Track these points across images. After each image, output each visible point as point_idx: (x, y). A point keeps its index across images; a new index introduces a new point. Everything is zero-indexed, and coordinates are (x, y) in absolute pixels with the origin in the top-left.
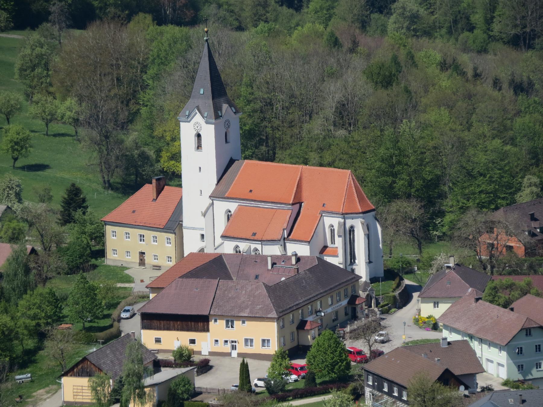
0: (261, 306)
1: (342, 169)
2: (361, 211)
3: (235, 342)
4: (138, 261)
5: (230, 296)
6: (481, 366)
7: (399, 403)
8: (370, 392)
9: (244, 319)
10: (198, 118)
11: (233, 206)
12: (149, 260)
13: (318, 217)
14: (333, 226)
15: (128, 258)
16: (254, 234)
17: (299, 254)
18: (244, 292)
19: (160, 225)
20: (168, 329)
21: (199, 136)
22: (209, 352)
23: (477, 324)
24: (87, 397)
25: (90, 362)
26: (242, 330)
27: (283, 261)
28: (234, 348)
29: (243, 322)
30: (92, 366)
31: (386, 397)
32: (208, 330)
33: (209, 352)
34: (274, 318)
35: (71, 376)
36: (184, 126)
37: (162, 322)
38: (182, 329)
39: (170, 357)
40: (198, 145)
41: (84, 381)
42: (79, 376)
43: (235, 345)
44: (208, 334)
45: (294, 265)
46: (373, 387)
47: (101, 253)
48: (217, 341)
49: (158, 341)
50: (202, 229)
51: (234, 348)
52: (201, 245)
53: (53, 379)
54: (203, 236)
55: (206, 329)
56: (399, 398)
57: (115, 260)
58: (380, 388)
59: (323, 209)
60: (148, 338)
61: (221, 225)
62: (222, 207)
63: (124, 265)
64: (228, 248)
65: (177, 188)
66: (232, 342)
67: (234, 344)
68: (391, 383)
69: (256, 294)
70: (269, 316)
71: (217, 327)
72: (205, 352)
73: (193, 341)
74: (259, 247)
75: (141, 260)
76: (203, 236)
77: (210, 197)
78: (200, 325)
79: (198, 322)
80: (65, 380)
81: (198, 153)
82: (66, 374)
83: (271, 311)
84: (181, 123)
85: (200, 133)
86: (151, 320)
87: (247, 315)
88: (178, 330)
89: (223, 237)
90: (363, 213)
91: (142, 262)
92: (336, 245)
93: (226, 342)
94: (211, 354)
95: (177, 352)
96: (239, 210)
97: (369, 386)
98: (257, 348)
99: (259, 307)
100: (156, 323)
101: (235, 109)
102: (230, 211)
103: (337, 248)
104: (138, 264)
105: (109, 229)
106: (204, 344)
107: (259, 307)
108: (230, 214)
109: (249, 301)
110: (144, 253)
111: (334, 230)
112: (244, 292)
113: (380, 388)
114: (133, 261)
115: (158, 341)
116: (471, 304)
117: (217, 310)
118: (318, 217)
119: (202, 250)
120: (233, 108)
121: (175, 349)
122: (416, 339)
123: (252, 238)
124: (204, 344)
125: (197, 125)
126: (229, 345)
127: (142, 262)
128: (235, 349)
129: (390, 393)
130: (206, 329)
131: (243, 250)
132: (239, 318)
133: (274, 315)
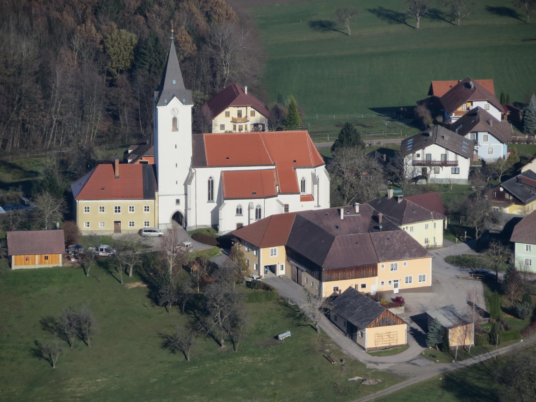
11: (216, 173)
28: (396, 286)
43: (397, 284)
44: (376, 277)
48: (383, 283)
51: (396, 286)
62: (204, 174)
66: (395, 281)
81: (175, 133)
93: (390, 282)
112: (395, 240)
114: (108, 229)
126: (393, 283)
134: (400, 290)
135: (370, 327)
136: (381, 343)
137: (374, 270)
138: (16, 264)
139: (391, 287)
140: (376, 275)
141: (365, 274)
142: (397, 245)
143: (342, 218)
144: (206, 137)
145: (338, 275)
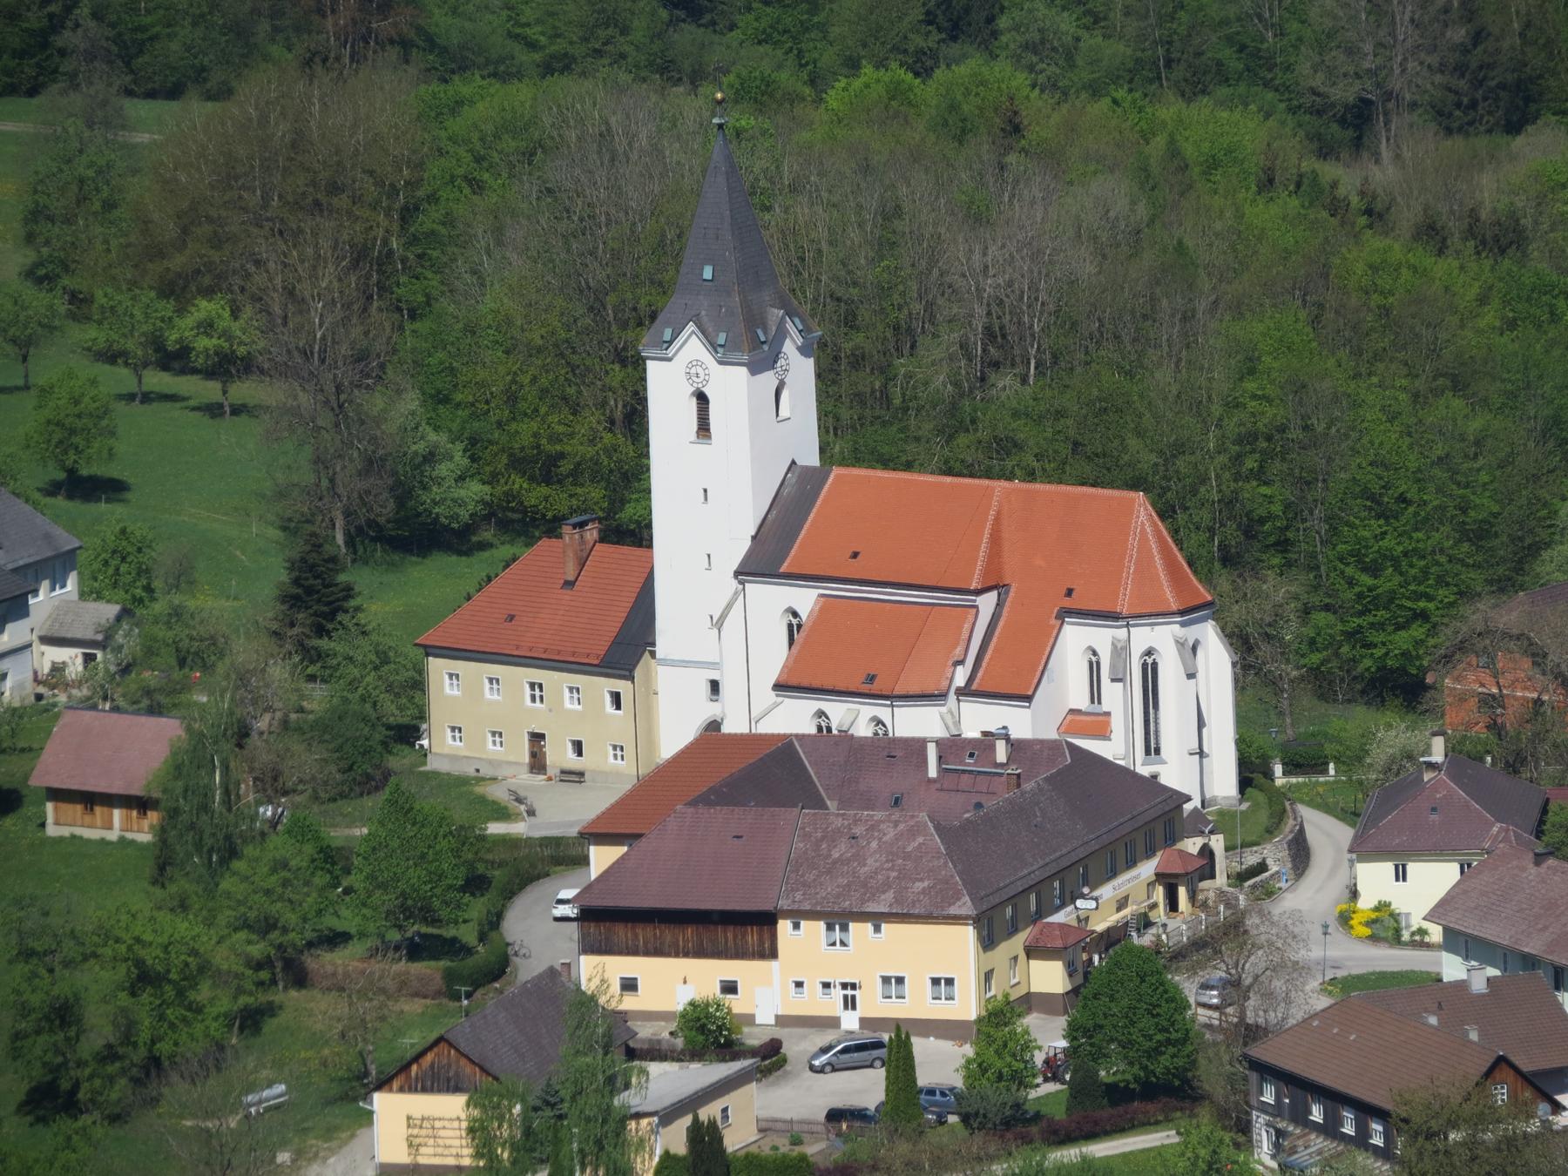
0: (926, 883)
1: (1093, 486)
2: (1174, 607)
3: (853, 986)
4: (526, 759)
5: (836, 855)
6: (620, 1012)
7: (1363, 1159)
8: (1268, 1124)
9: (877, 919)
10: (692, 348)
11: (805, 599)
12: (559, 755)
13: (1053, 627)
14: (1095, 653)
15: (491, 748)
16: (871, 679)
17: (1015, 734)
18: (874, 844)
19: (574, 654)
20: (657, 952)
21: (702, 399)
22: (777, 1017)
23: (1545, 928)
24: (456, 1149)
25: (457, 1050)
26: (874, 950)
27: (971, 755)
28: (850, 1003)
29: (877, 929)
30: (463, 1061)
31: (1318, 1142)
32: (773, 954)
33: (777, 1017)
34: (967, 918)
35: (401, 1090)
36: (655, 371)
37: (639, 931)
38: (700, 953)
39: (662, 1032)
40: (722, 433)
41: (452, 1106)
42: (424, 1090)
43: (853, 997)
44: (774, 964)
45: (1002, 765)
46: (1276, 1111)
47: (408, 734)
48: (799, 985)
49: (629, 985)
50: (714, 665)
51: (850, 1003)
52: (711, 710)
53: (347, 1097)
54: (715, 686)
55: (769, 952)
56: (1362, 1140)
57: (454, 758)
58: (1300, 1116)
59: (1067, 603)
60: (598, 973)
61: (773, 656)
62: (775, 602)
63: (486, 771)
64: (794, 718)
65: (638, 552)
66: (844, 986)
67: (849, 992)
68: (1334, 1099)
69: (909, 849)
70: (953, 911)
71: (800, 941)
72: (765, 1017)
73: (730, 988)
74: (884, 713)
75: (533, 755)
76: (715, 686)
77: (737, 574)
78: (752, 936)
79: (745, 930)
80: (381, 1102)
81: (702, 448)
82: (383, 1084)
83: (957, 897)
84: (649, 363)
85: (706, 390)
86: (609, 923)
87: (886, 910)
88: (686, 955)
89: (780, 687)
90: (1182, 613)
91: (537, 763)
92: (1105, 707)
93: (826, 985)
94: (782, 1021)
95: (684, 1015)
96: (827, 607)
97: (1264, 1108)
98: (918, 1004)
99: (919, 886)
100: (621, 932)
101: (802, 321)
102: (795, 614)
103: (1108, 714)
104: (526, 769)
105: (437, 667)
106: (764, 993)
107: (919, 886)
108: (795, 622)
109: (892, 869)
110: (542, 736)
111: (1098, 663)
112: (874, 844)
113: (1300, 1116)
114: (511, 758)
115: (629, 985)
116: (1523, 869)
117: (798, 896)
118: (1053, 627)
119: (714, 726)
120: (797, 320)
121: (680, 1008)
122: (1355, 972)
123: (865, 688)
124: (764, 993)
125: (700, 370)
126: (838, 994)
127: (537, 763)
128: (854, 1008)
129: (1330, 1128)
130: (769, 952)
131: (840, 725)
132: (862, 917)
133: (965, 906)
134: (864, 1022)
135: (391, 1090)
136: (430, 1150)
137: (766, 936)
138: (57, 823)
139: (832, 1004)
140: (773, 954)
141: (731, 943)
142: (870, 861)
143: (933, 772)
144: (837, 476)
145: (636, 936)
